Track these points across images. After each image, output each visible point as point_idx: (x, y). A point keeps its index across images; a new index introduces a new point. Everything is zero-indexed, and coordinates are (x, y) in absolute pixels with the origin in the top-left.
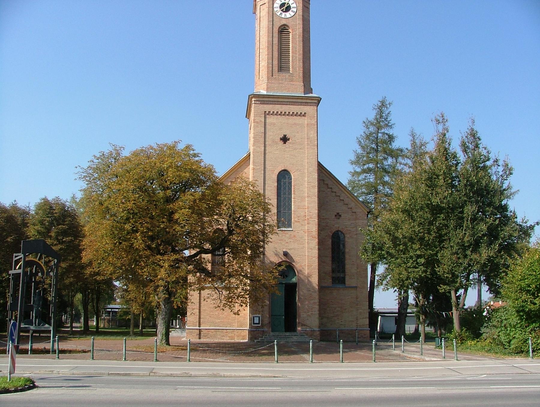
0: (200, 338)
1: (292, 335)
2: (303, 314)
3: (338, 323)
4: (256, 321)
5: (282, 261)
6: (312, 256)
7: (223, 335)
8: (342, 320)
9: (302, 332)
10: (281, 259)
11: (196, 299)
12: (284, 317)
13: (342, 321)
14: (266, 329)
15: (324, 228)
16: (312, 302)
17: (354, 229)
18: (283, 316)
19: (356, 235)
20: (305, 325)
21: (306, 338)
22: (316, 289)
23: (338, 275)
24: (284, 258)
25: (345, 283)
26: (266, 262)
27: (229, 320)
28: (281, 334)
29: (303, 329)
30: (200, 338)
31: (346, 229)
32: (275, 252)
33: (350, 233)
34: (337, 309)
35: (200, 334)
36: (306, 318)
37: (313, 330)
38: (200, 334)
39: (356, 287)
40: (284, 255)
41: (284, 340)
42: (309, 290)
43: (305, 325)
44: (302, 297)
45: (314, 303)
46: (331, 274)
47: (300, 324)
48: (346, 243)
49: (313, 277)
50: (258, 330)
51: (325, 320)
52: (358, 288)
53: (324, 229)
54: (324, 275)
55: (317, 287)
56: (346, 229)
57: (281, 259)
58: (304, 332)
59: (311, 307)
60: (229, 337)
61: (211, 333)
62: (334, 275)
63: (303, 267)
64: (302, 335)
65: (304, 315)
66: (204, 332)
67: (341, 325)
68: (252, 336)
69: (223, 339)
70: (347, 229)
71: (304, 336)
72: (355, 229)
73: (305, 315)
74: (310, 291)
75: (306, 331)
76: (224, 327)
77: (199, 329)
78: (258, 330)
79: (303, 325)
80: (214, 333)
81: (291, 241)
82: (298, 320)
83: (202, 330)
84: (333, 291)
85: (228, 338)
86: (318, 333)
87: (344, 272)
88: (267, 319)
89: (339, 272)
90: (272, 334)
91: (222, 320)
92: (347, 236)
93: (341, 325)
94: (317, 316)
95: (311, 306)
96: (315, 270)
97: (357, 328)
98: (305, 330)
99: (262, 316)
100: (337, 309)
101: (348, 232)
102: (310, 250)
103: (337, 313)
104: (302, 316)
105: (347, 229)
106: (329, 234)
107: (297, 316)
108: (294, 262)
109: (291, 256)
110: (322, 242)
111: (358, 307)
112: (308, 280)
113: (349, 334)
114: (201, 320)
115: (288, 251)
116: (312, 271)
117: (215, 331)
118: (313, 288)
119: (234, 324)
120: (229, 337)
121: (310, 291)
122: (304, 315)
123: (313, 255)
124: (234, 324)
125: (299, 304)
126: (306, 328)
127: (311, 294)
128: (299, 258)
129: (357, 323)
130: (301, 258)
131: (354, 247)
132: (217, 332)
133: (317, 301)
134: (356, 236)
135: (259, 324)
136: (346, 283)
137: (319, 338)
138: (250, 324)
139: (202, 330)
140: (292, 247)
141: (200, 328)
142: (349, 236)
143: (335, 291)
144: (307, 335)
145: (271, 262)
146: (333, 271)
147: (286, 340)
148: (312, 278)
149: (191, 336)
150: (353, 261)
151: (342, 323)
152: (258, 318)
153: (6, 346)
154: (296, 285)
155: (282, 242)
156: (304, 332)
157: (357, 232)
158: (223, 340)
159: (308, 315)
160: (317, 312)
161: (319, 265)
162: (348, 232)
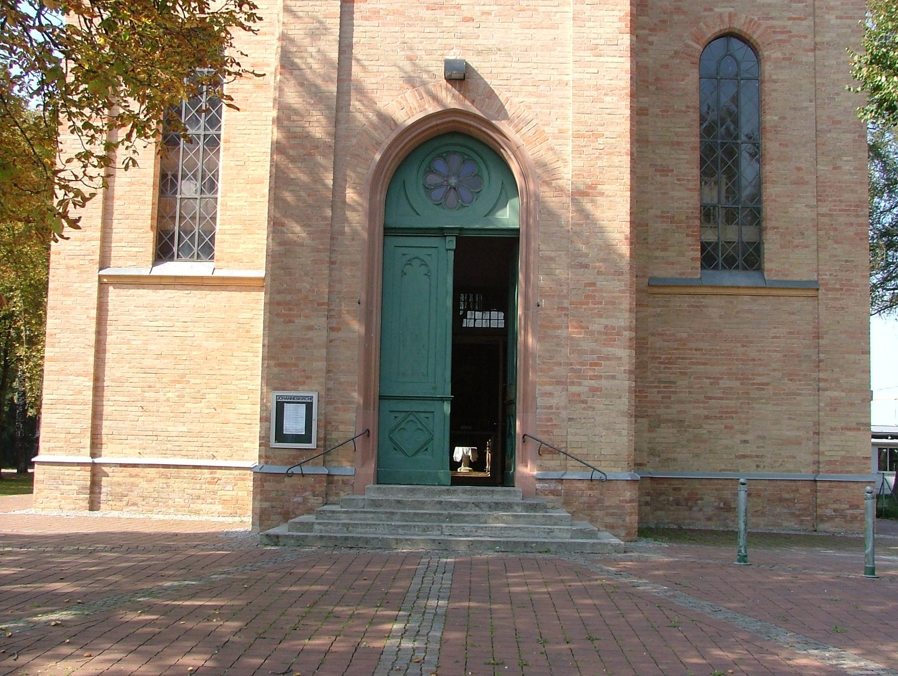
0: (94, 505)
1: (477, 505)
2: (548, 388)
3: (726, 447)
4: (294, 423)
5: (439, 109)
6: (597, 88)
7: (197, 492)
8: (745, 437)
9: (539, 486)
10: (435, 99)
11: (84, 331)
12: (447, 408)
13: (745, 442)
14: (345, 468)
15: (665, 17)
16: (597, 325)
17: (804, 23)
18: (442, 399)
19: (814, 50)
20: (555, 451)
21: (558, 521)
22: (621, 256)
23: (731, 233)
24: (450, 99)
25: (760, 269)
26: (359, 116)
27: (227, 428)
28: (420, 497)
29: (547, 469)
30: (94, 505)
31: (765, 24)
32: (408, 67)
33: (784, 41)
34: (725, 383)
35: (95, 486)
36: (564, 414)
37: (596, 476)
38: (95, 486)
39: (811, 288)
40: (449, 79)
41: (425, 529)
42: (580, 260)
43: (555, 451)
44: (543, 303)
45: (610, 334)
46: (697, 222)
47: (532, 447)
48: (767, 87)
49: (602, 194)
50: (297, 470)
51: (666, 433)
52: (822, 291)
53: (664, 21)
54: (665, 226)
55: (625, 249)
56: (765, 24)
57: (435, 99)
58: (553, 486)
59: (593, 352)
60: (224, 502)
61: (144, 484)
62: (710, 236)
63: (552, 142)
64: (534, 507)
65: (550, 394)
66: (115, 479)
67: (744, 457)
68: (266, 505)
69: (197, 513)
70: (774, 23)
71: (544, 508)
72: (808, 23)
73: (559, 399)
74: (586, 266)
75: (560, 480)
76: (202, 457)
77: (94, 464)
78: (297, 470)
79: (546, 450)
80: (159, 483)
81: (489, 14)
82: (523, 424)
83: (105, 469)
84: (706, 301)
85: (219, 508)
86: (628, 495)
87: (756, 216)
88: (351, 416)
89: (730, 218)
90: (374, 492)
91: (196, 427)
92: (771, 54)
93: (744, 457)
94: (624, 403)
95: (593, 345)
96: (616, 160)
97: (818, 472)
98: (555, 475)
99: (328, 398)
100: (725, 383)
101: (779, 37)
102: (588, 57)
103: (724, 402)
104: (540, 401)
105: (774, 23)
106: (687, 46)
107: (519, 406)
108: (506, 117)
109: (486, 83)
110: (657, 79)
111: (822, 375)
112: (581, 211)
113: (781, 500)
114: (105, 423)
115: (474, 62)
116: (600, 163)
117: (162, 475)
118: (608, 248)
119: (246, 445)
120: (224, 502)
121: (586, 266)
122: (550, 394)
123: (605, 82)
124: (246, 445)
125: (530, 340)
126: (565, 468)
127: (594, 284)
128: (530, 94)
129: (818, 453)
130: (540, 96)
131: (805, 104)
132: (172, 481)
133: (622, 323)
134: (811, 54)
135: (306, 438)
136: (767, 265)
137: (632, 520)
138: (264, 442)
139: (105, 469)
140: (491, 43)
141: (97, 460)
142: (779, 55)
143: (716, 301)
144: (567, 503)
145: (385, 120)
146: (707, 214)
147: (435, 535)
148: (599, 199)
149: (58, 494)
150: (799, 169)
151: (749, 450)
152: (302, 408)
153: (890, 470)
154: (517, 240)
155: (439, 14)
156: (553, 486)
157: (818, 39)
158: (196, 518)
159: (575, 399)
160: (624, 383)
161: (638, 114)
162: (779, 37)
